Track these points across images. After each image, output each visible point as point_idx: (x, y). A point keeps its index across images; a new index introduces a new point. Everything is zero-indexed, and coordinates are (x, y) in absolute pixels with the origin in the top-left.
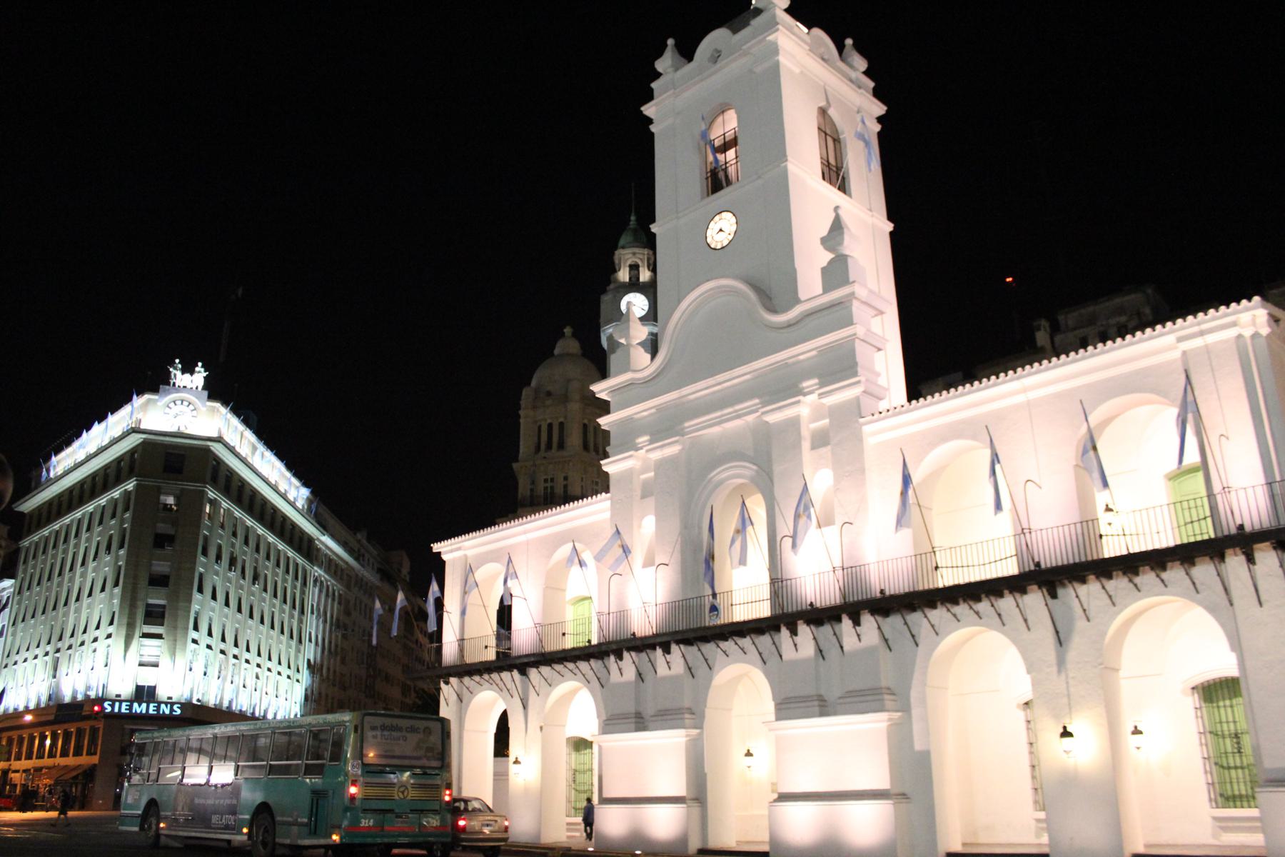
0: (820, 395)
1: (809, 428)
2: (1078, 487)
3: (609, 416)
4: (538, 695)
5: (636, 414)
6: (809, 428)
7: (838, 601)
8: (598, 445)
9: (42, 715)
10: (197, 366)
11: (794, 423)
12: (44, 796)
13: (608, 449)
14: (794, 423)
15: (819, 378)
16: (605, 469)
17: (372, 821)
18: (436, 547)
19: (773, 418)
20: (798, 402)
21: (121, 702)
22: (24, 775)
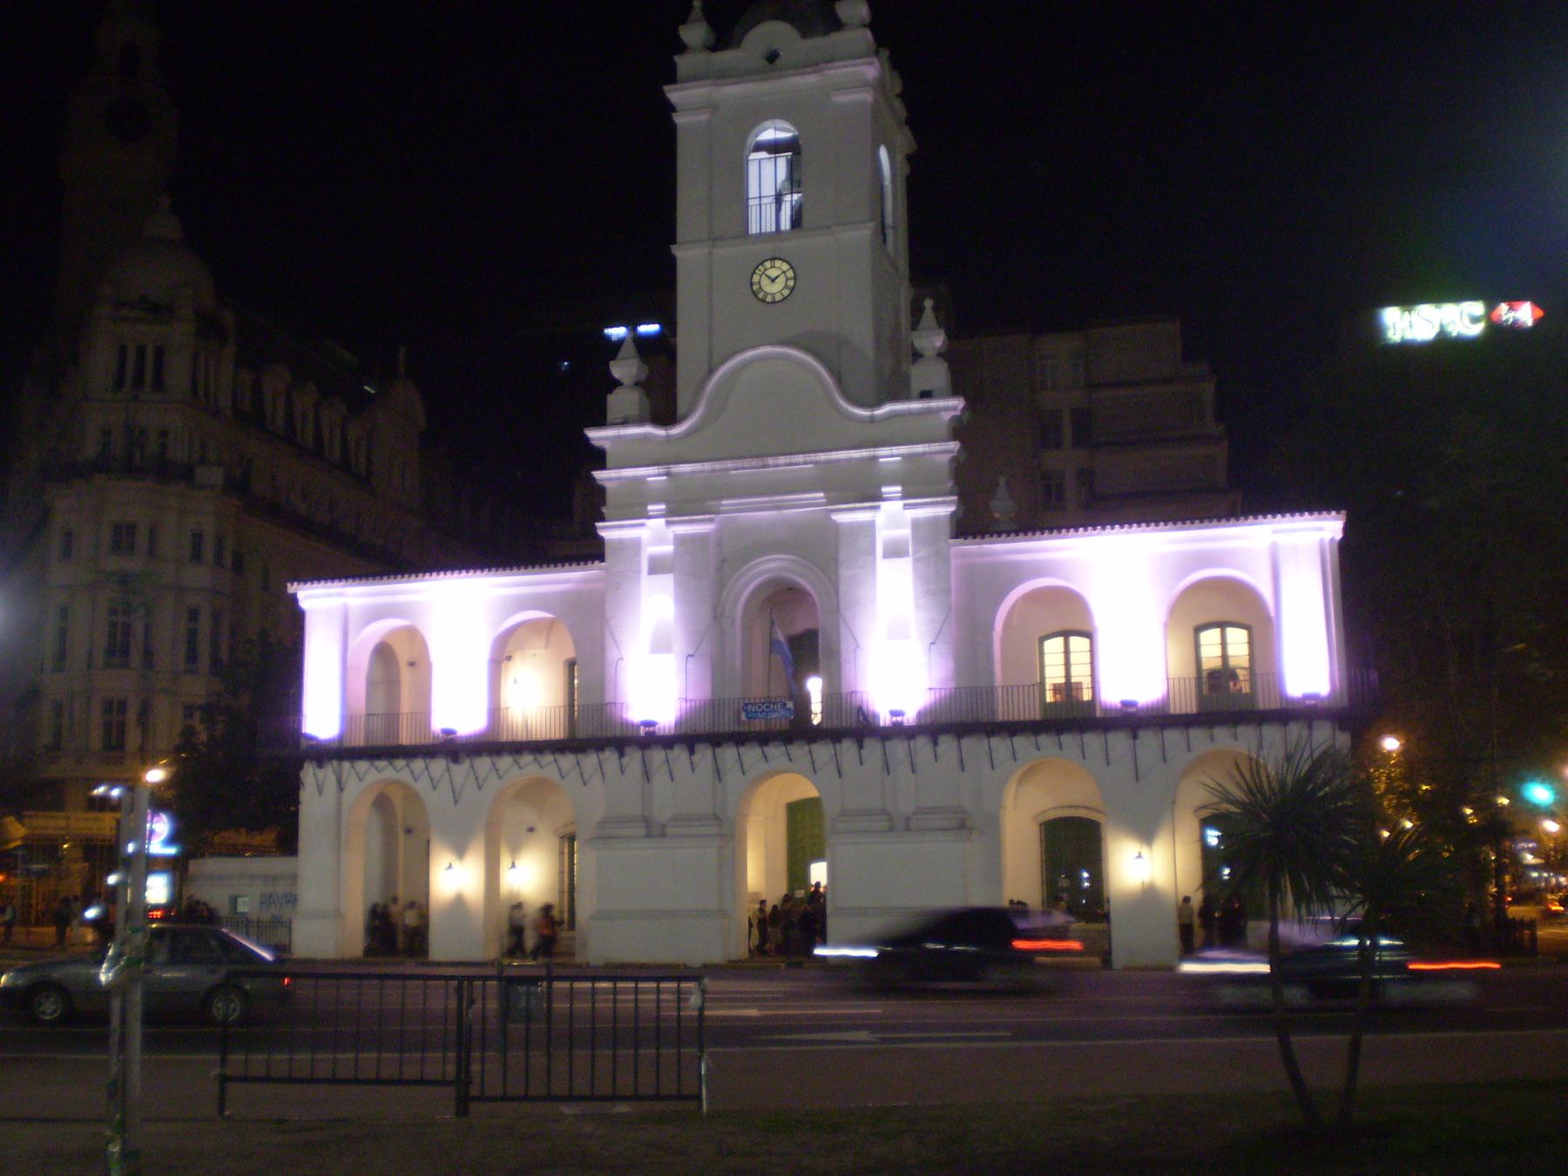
0: (905, 505)
1: (883, 535)
2: (500, 676)
3: (604, 472)
4: (456, 802)
5: (649, 476)
6: (650, 550)
7: (707, 728)
8: (595, 503)
9: (987, 692)
10: (682, 48)
11: (871, 526)
12: (1553, 865)
13: (604, 510)
14: (636, 545)
15: (903, 486)
16: (602, 533)
17: (1360, 911)
18: (292, 588)
19: (842, 518)
20: (643, 525)
21: (774, 710)
22: (97, 890)
